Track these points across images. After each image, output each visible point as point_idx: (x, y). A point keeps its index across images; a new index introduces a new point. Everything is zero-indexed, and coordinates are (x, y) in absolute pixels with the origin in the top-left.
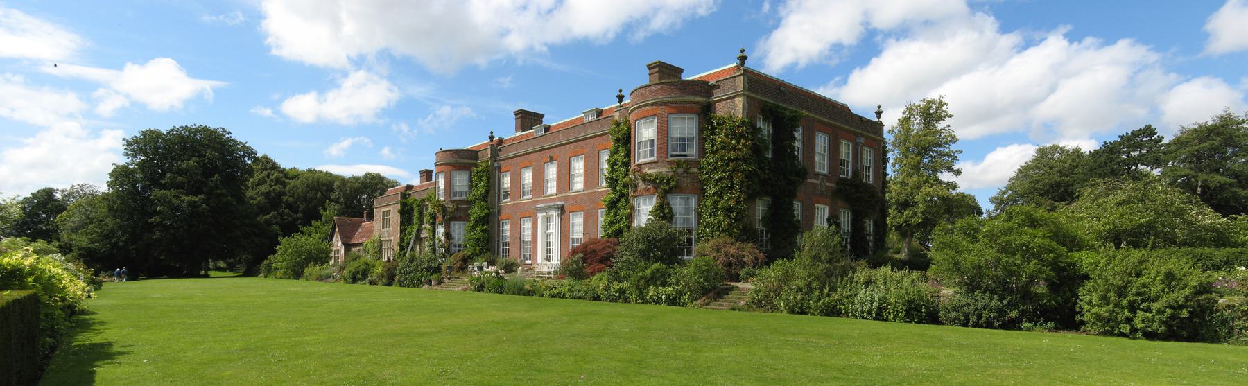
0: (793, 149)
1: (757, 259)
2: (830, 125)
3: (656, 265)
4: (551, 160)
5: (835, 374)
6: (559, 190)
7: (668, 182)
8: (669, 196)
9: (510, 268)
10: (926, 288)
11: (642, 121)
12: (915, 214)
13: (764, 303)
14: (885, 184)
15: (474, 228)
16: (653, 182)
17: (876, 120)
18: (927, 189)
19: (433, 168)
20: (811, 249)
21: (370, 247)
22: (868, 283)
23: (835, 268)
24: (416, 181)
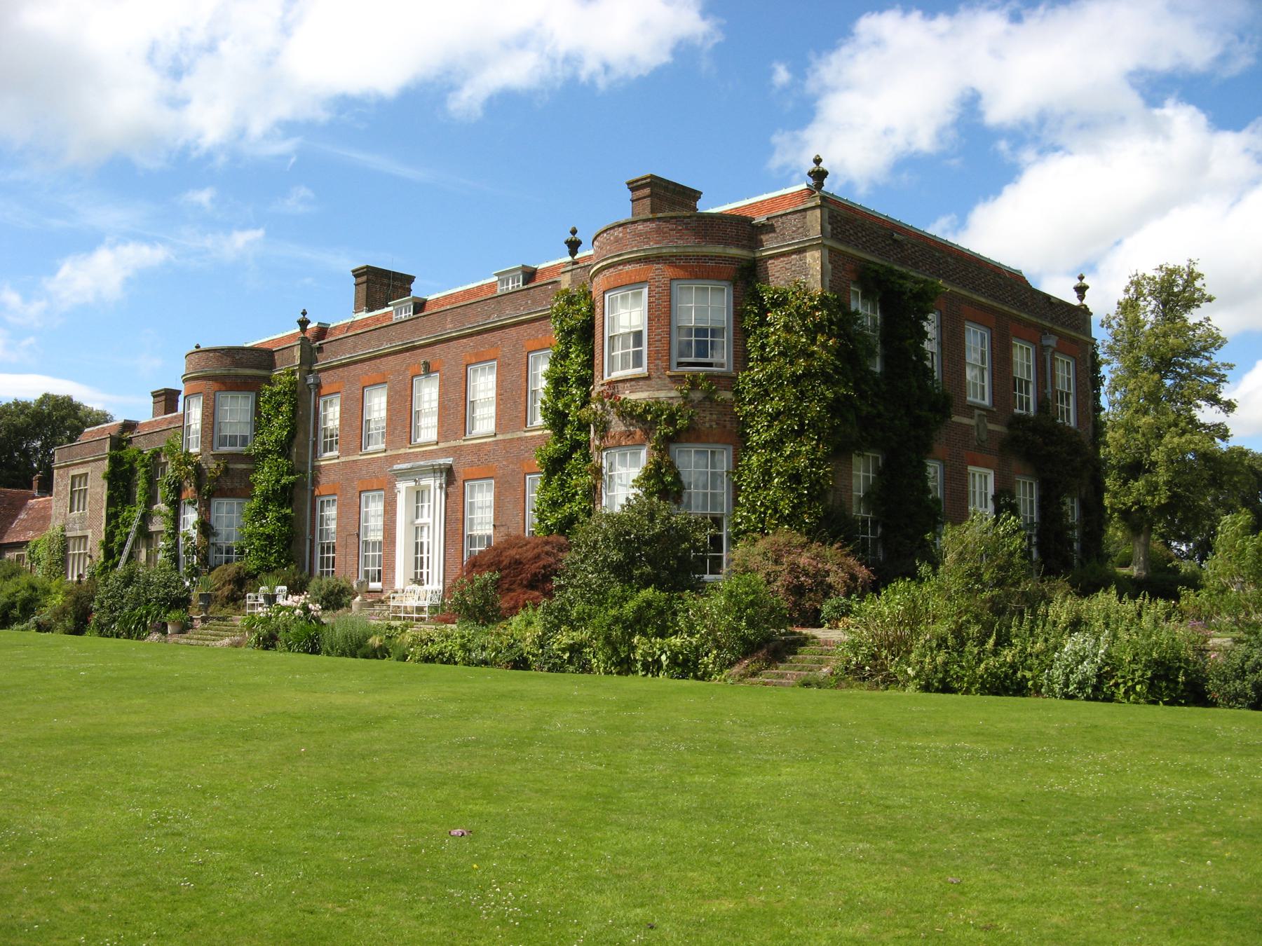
0: (922, 355)
1: (853, 577)
2: (992, 310)
3: (648, 593)
4: (428, 370)
5: (1005, 812)
6: (443, 434)
7: (671, 420)
8: (674, 448)
9: (335, 599)
10: (1181, 631)
11: (618, 294)
12: (1153, 489)
13: (869, 671)
14: (1098, 428)
15: (260, 513)
16: (641, 418)
17: (1076, 302)
18: (1171, 440)
19: (179, 385)
20: (961, 558)
21: (41, 552)
22: (1076, 624)
23: (1009, 596)
24: (142, 410)
